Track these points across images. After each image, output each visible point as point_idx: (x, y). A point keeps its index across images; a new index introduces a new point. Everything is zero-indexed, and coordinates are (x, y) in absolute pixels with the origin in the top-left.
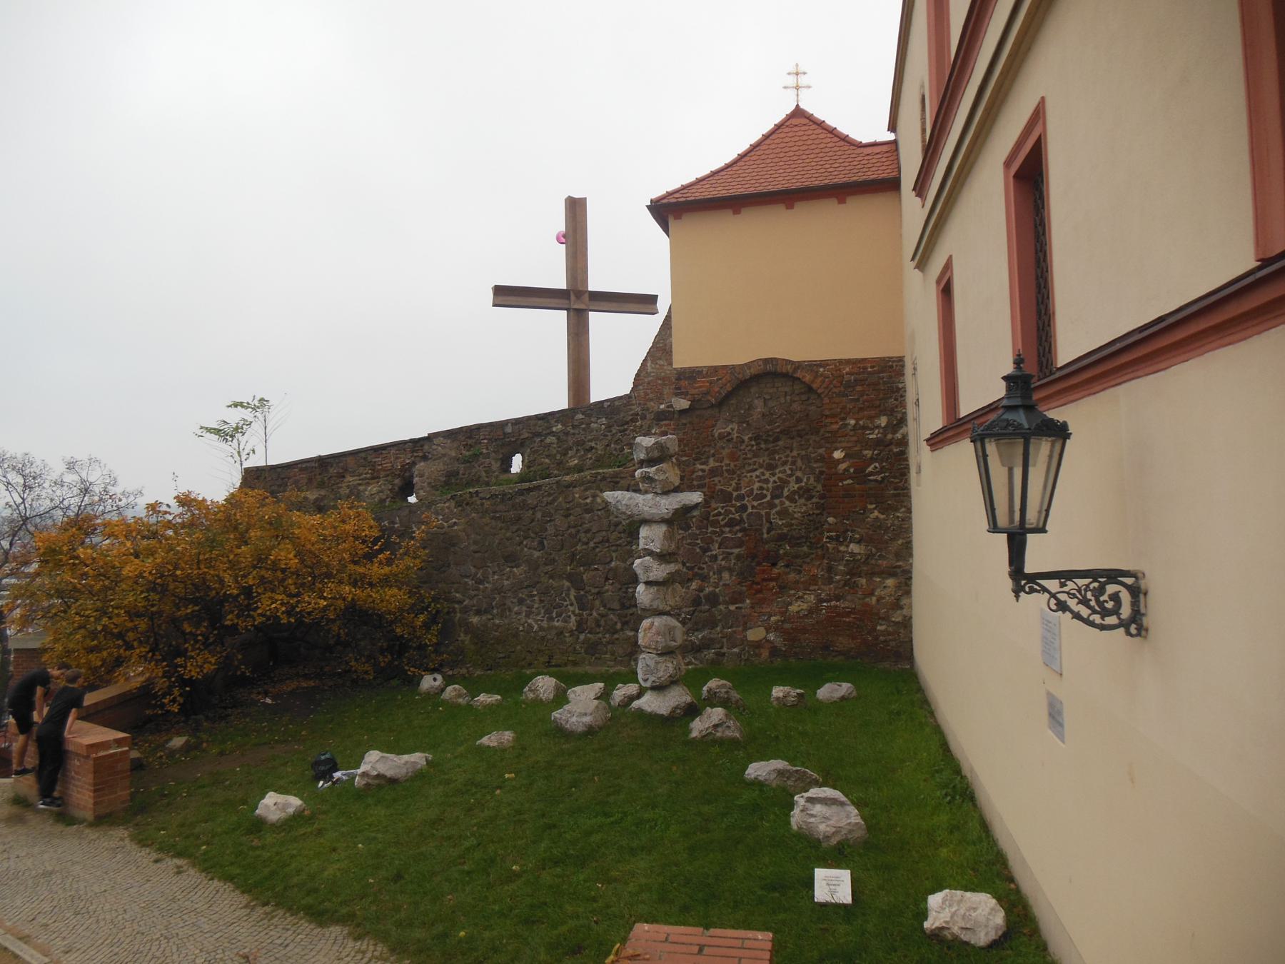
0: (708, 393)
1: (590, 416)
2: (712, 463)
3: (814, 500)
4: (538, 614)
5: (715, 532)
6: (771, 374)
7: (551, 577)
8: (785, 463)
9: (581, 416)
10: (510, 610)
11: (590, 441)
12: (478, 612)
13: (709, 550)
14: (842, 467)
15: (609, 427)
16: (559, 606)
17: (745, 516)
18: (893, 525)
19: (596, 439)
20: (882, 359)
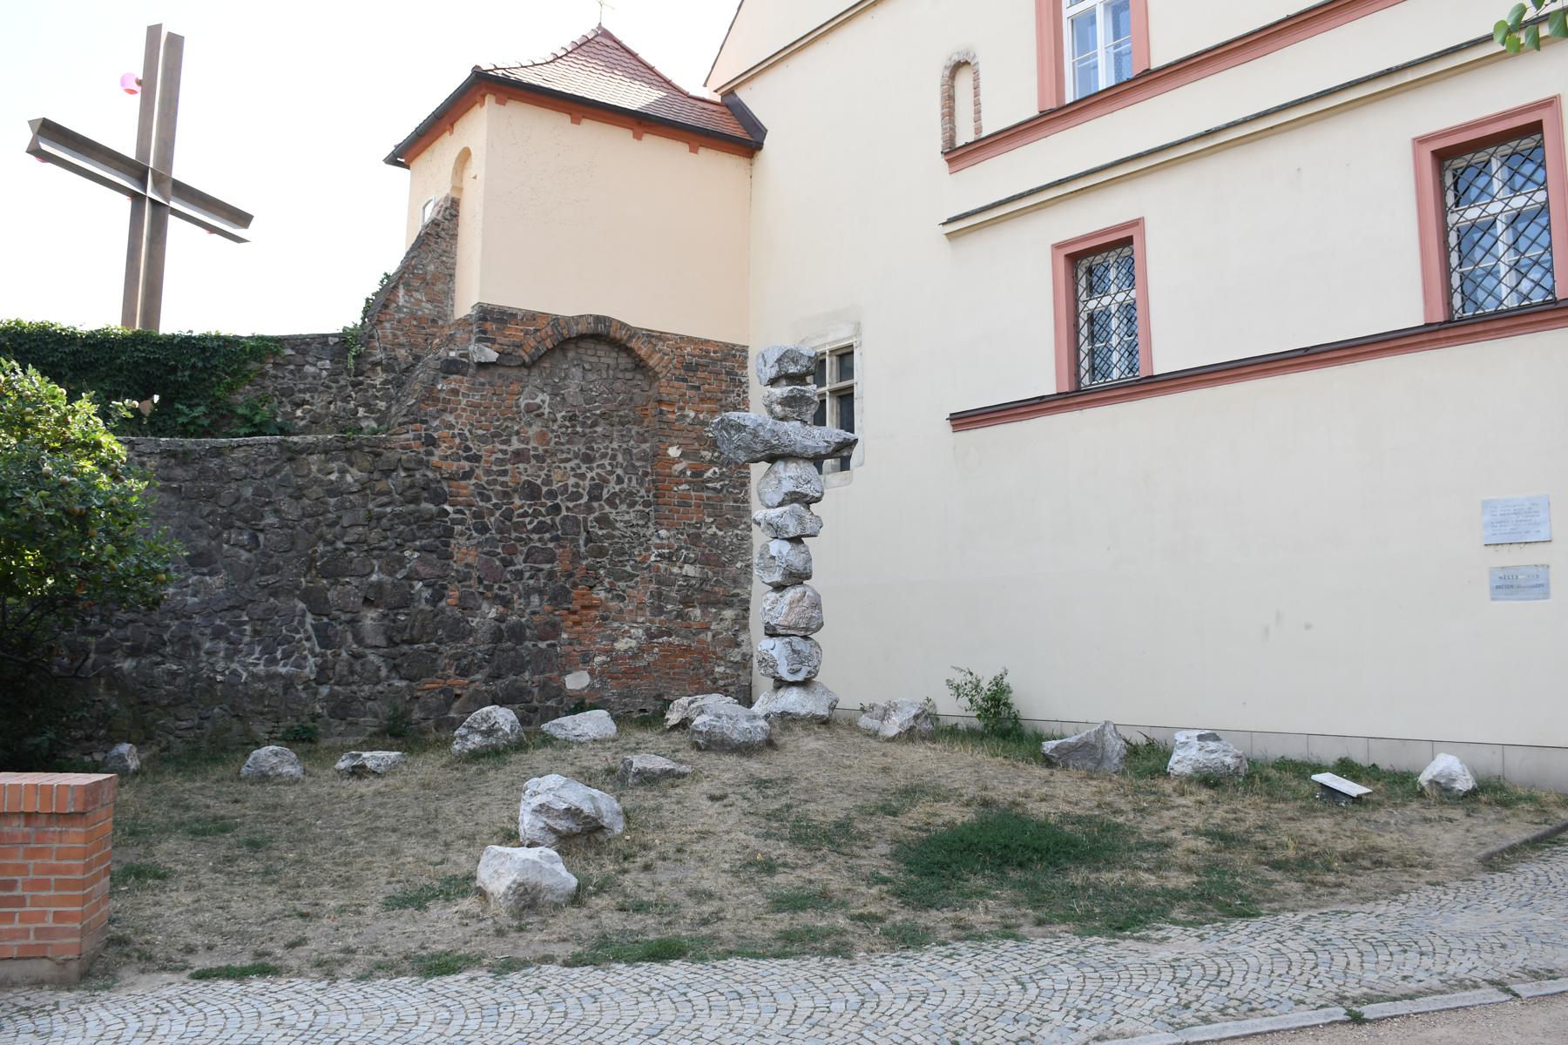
0: (520, 346)
1: (304, 353)
2: (516, 444)
3: (638, 507)
4: (250, 654)
5: (519, 540)
6: (601, 336)
7: (275, 594)
8: (604, 456)
9: (289, 352)
10: (197, 646)
11: (303, 391)
12: (134, 652)
13: (512, 563)
14: (678, 467)
15: (334, 375)
16: (288, 640)
17: (558, 519)
18: (731, 543)
19: (312, 390)
20: (726, 345)
